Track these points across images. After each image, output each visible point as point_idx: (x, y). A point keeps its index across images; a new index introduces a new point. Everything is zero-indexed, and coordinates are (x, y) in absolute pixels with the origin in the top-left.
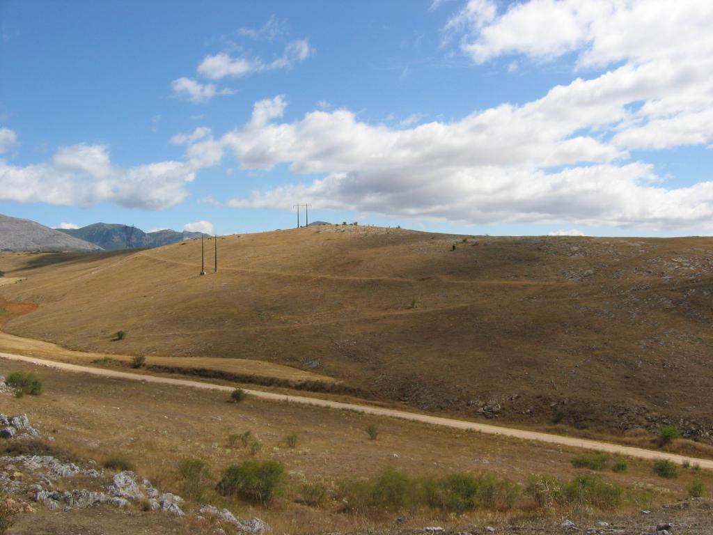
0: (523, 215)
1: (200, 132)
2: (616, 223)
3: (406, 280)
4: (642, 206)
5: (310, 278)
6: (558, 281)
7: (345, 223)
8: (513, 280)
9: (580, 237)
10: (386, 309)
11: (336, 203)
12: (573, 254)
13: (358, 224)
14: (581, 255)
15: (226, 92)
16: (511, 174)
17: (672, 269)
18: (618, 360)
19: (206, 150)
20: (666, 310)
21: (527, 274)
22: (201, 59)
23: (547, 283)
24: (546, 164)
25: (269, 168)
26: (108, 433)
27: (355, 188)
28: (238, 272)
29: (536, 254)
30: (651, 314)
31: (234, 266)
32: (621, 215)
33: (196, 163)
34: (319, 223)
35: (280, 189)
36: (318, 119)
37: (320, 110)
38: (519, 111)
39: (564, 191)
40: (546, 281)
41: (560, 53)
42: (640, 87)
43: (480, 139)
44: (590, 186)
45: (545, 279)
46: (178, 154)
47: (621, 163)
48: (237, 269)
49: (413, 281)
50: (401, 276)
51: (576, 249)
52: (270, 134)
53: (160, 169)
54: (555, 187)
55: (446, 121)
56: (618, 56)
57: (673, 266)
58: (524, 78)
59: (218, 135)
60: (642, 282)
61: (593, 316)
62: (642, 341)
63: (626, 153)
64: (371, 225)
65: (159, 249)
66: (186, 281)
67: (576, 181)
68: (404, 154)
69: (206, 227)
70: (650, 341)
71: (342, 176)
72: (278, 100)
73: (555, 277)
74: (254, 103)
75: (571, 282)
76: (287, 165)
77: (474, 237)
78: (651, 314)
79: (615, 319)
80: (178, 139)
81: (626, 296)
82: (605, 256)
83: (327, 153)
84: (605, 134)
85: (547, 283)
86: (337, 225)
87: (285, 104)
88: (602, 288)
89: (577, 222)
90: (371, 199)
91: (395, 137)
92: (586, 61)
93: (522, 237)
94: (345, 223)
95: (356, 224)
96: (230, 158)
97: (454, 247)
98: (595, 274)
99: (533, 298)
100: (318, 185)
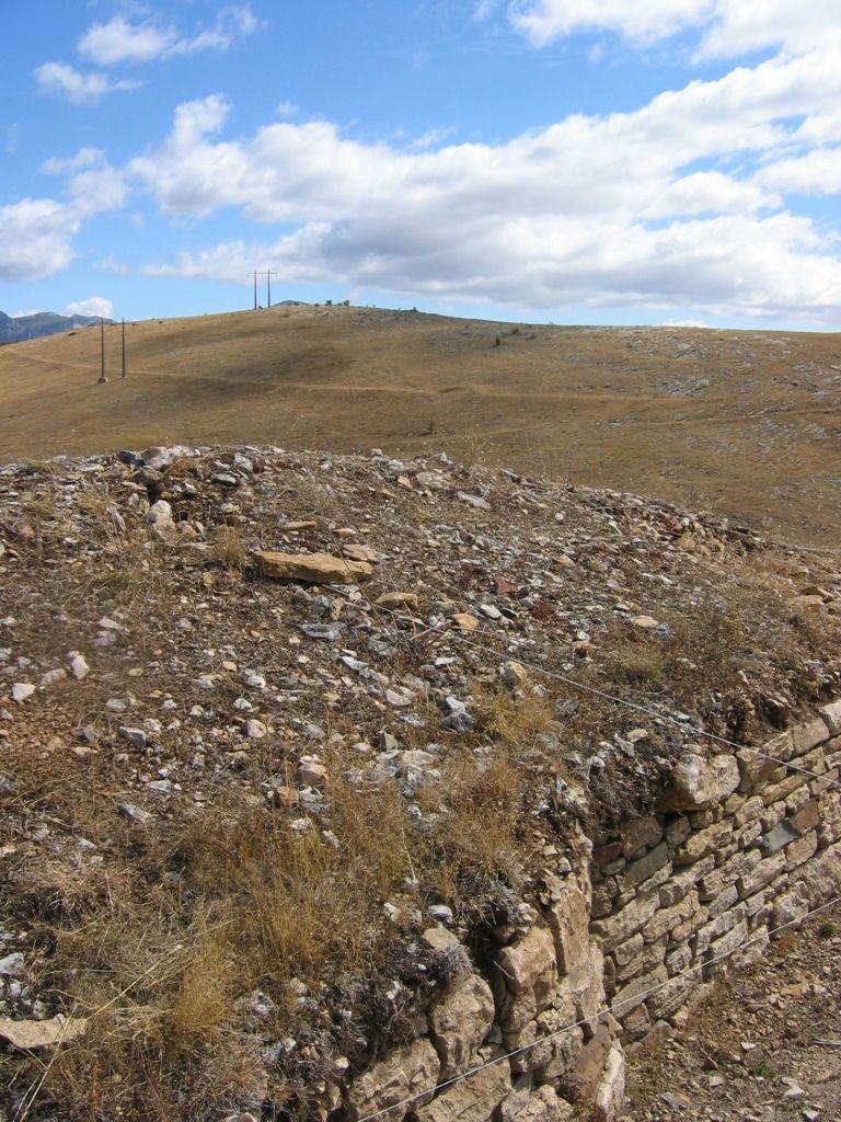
0: (612, 296)
1: (87, 154)
2: (759, 312)
3: (421, 391)
4: (797, 280)
6: (656, 395)
9: (695, 330)
10: (389, 436)
11: (314, 271)
12: (681, 354)
14: (694, 357)
15: (124, 85)
16: (585, 230)
17: (829, 380)
18: (737, 515)
19: (101, 186)
20: (816, 442)
21: (608, 384)
22: (84, 29)
24: (651, 213)
25: (204, 212)
27: (342, 249)
28: (159, 378)
29: (625, 352)
30: (793, 448)
31: (155, 368)
32: (766, 299)
33: (84, 206)
34: (289, 303)
35: (222, 248)
36: (281, 136)
37: (280, 120)
38: (601, 127)
39: (675, 258)
40: (637, 395)
41: (666, 31)
42: (794, 94)
43: (537, 171)
44: (716, 250)
45: (636, 392)
46: (54, 188)
47: (764, 213)
48: (158, 373)
49: (432, 393)
50: (415, 386)
51: (686, 346)
52: (202, 157)
53: (29, 211)
54: (662, 251)
55: (488, 138)
56: (764, 39)
57: (831, 376)
58: (607, 73)
59: (119, 161)
60: (782, 400)
61: (705, 449)
62: (776, 488)
65: (33, 343)
66: (76, 392)
67: (693, 242)
68: (422, 196)
69: (101, 307)
70: (788, 488)
71: (324, 228)
72: (212, 102)
73: (653, 390)
74: (175, 107)
75: (676, 397)
76: (265, 205)
77: (530, 326)
78: (793, 448)
79: (736, 454)
80: (53, 166)
81: (757, 420)
82: (731, 358)
83: (300, 190)
84: (743, 164)
85: (638, 399)
86: (317, 305)
87: (225, 108)
88: (722, 408)
89: (697, 307)
90: (372, 264)
91: (406, 165)
92: (714, 45)
93: (468, 323)
94: (329, 302)
95: (346, 303)
96: (141, 197)
97: (498, 342)
98: (712, 385)
100: (287, 244)
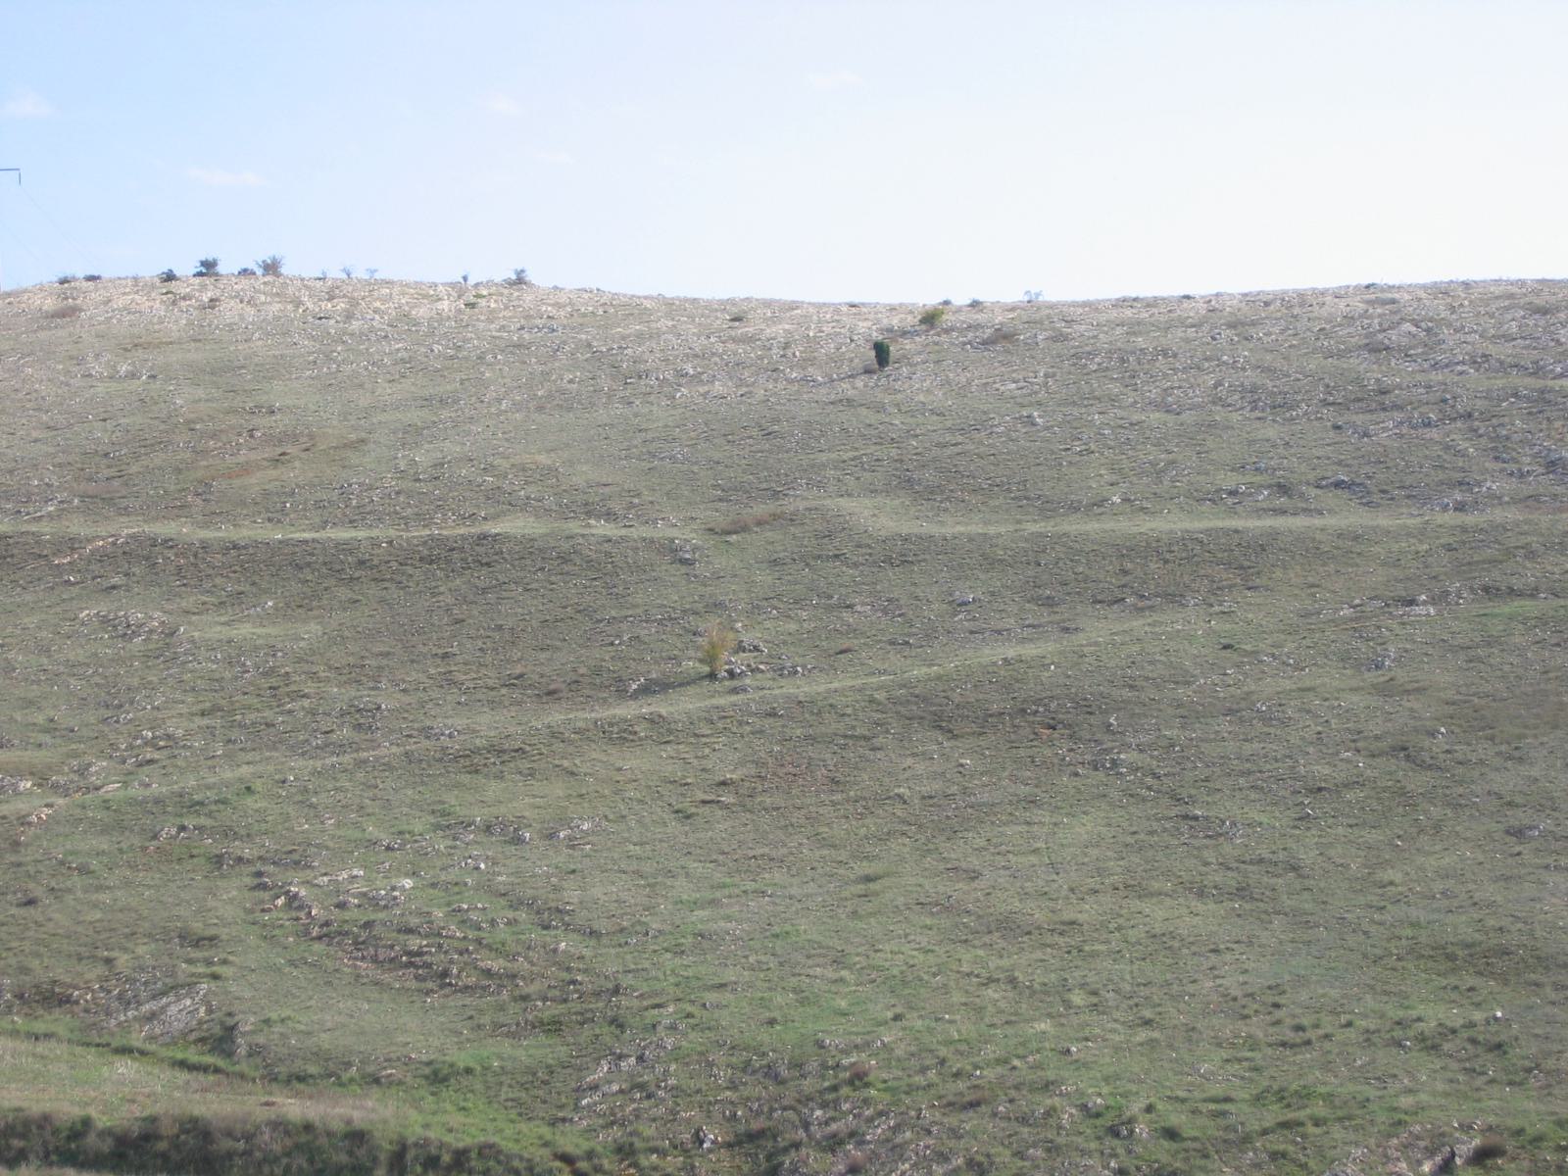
5: (72, 544)
7: (209, 267)
8: (1260, 512)
13: (284, 270)
23: (1470, 519)
26: (807, 819)
40: (1460, 507)
63: (110, 1141)
64: (360, 273)
94: (209, 267)
95: (271, 268)
97: (881, 352)
99: (1412, 602)
